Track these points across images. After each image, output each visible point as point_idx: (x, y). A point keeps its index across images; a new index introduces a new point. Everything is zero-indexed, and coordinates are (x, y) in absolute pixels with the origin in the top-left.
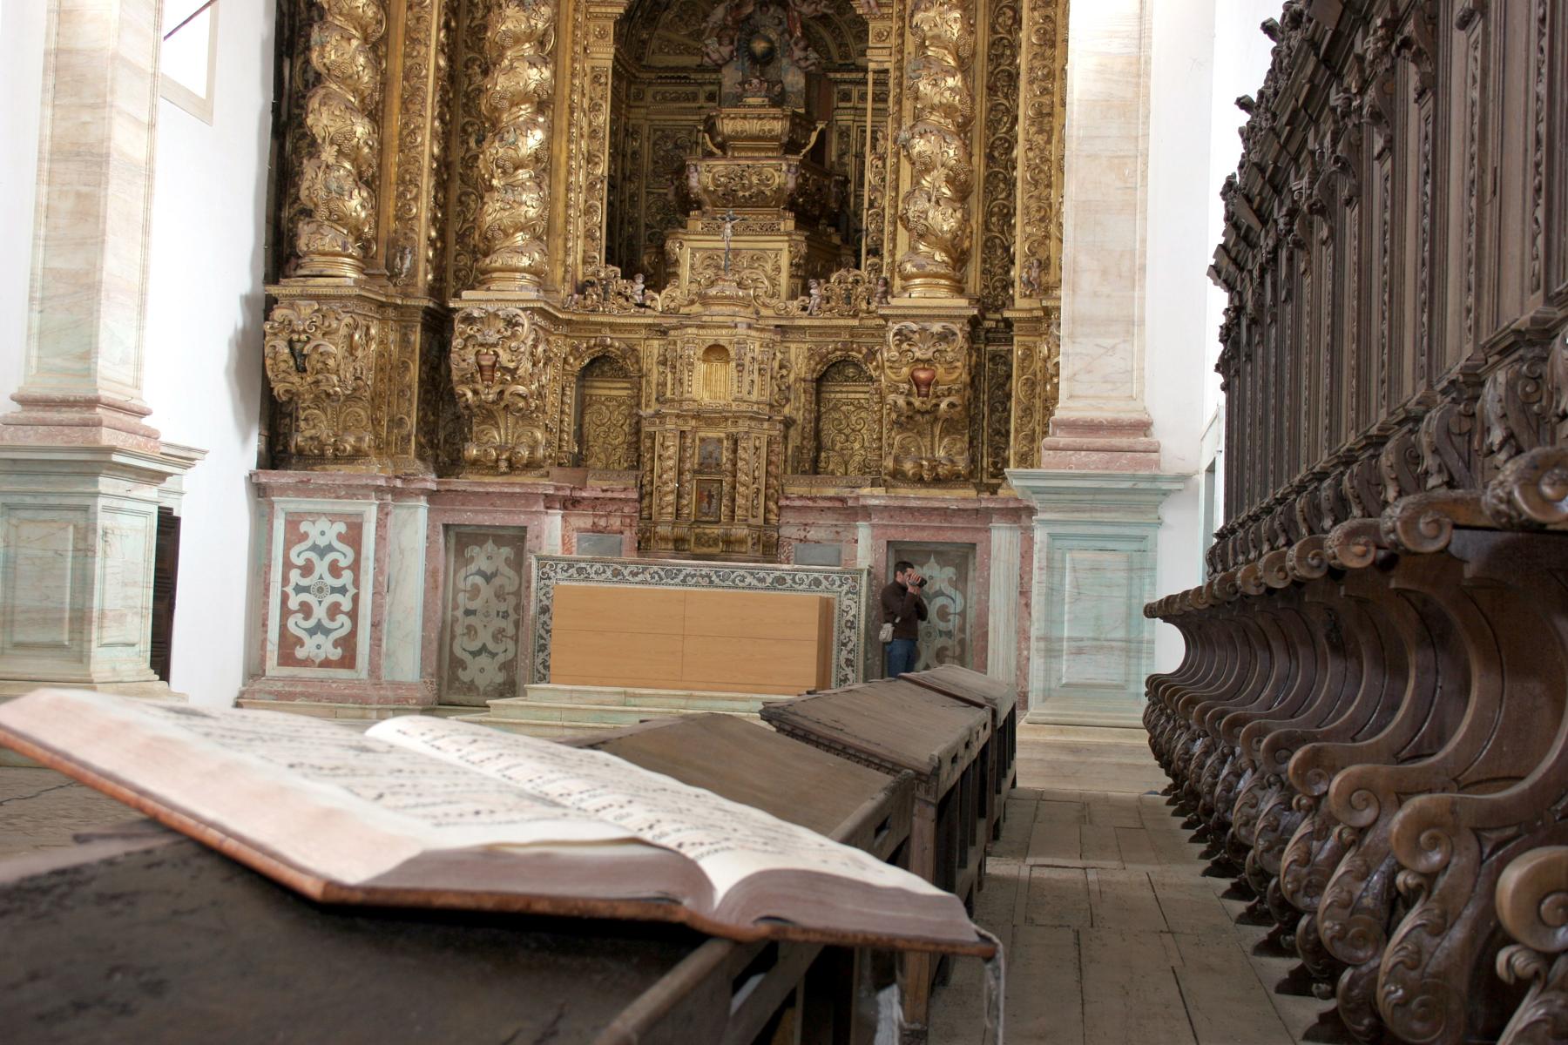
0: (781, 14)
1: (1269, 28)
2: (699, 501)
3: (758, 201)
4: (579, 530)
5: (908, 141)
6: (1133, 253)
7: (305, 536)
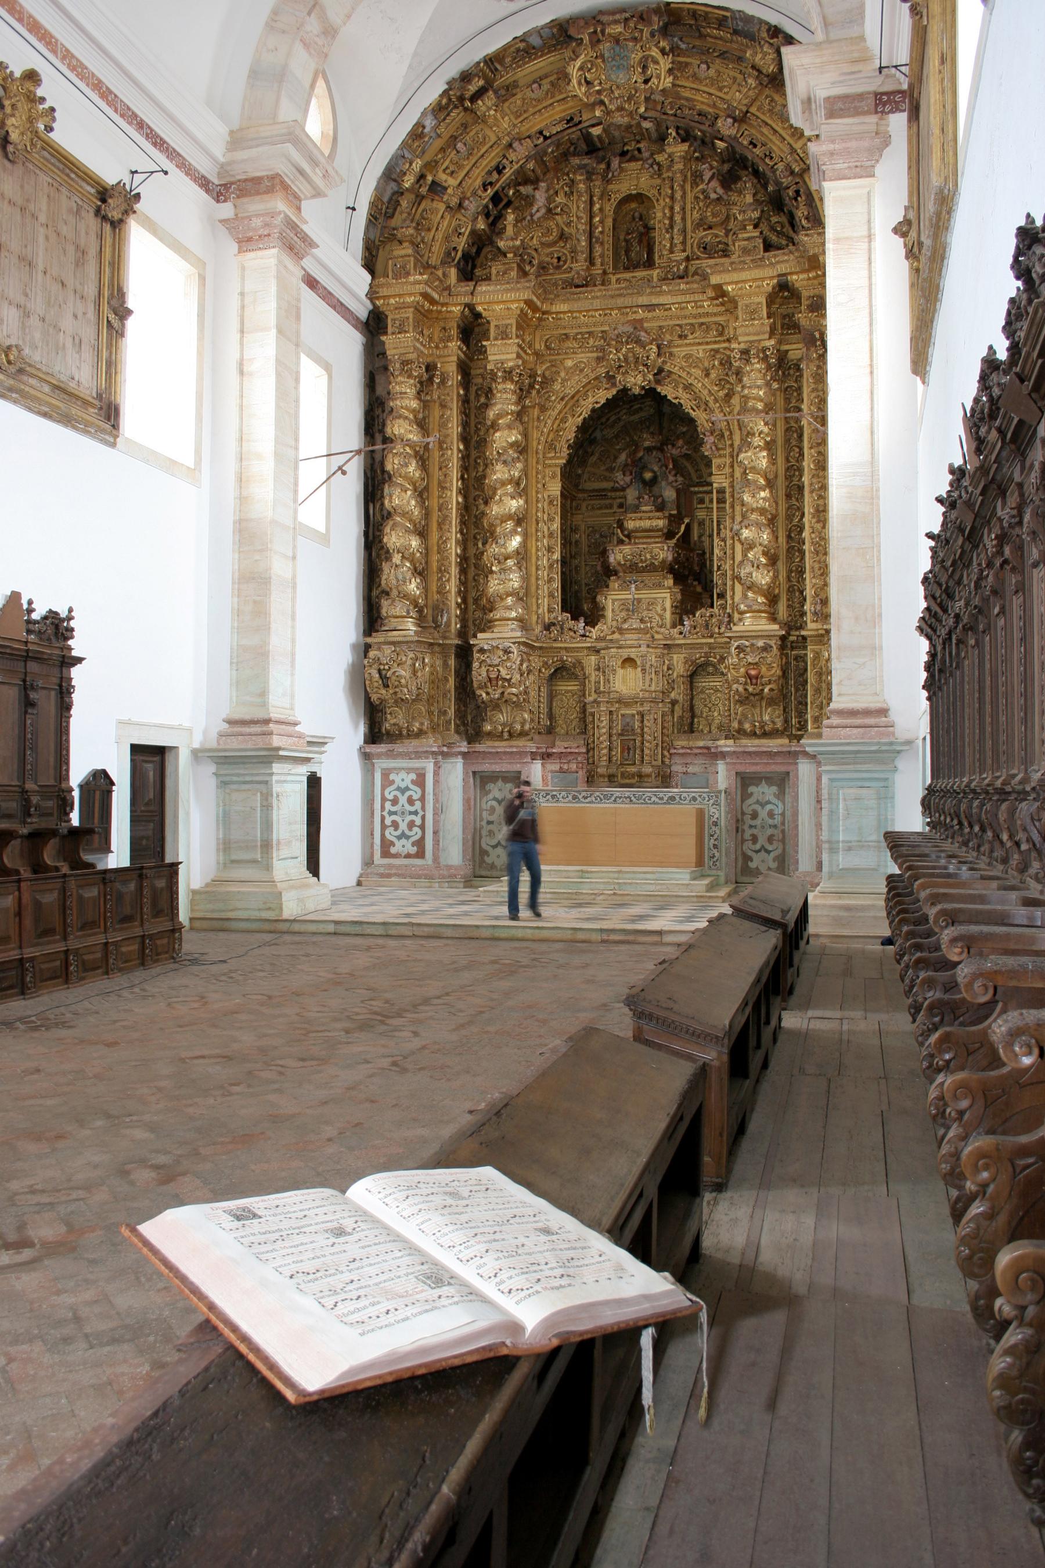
0: (660, 455)
1: (940, 500)
2: (622, 752)
3: (651, 568)
4: (552, 772)
5: (738, 531)
6: (873, 606)
7: (393, 782)
